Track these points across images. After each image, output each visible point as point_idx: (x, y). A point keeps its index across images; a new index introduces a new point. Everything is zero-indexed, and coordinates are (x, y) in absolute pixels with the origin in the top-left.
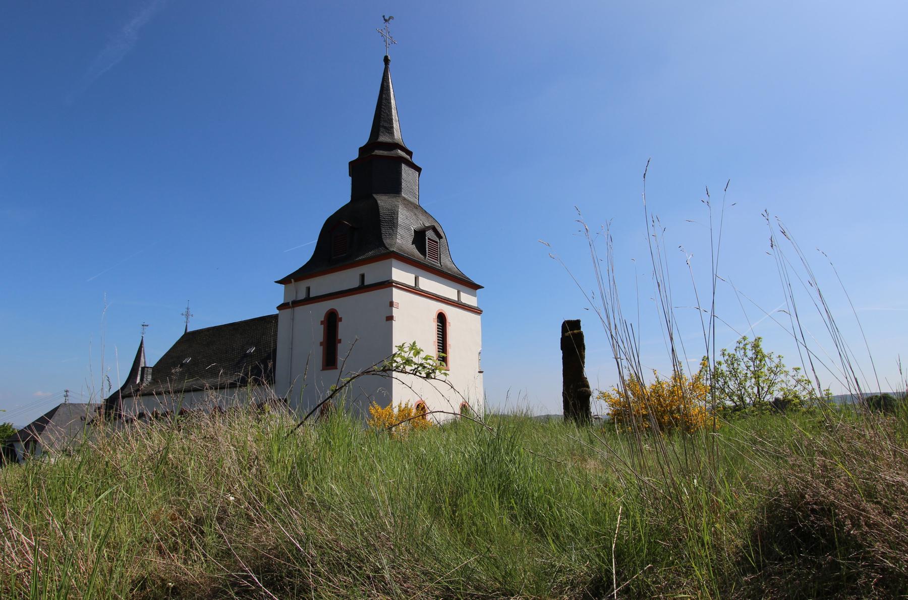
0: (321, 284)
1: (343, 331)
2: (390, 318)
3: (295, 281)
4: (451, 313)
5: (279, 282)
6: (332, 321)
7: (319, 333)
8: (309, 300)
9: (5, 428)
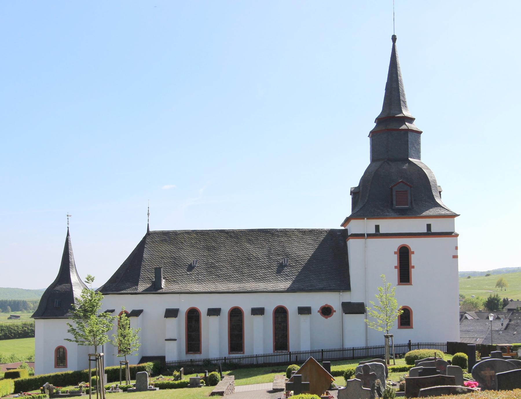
1: (414, 260)
2: (456, 257)
6: (404, 254)
7: (395, 260)
8: (377, 234)
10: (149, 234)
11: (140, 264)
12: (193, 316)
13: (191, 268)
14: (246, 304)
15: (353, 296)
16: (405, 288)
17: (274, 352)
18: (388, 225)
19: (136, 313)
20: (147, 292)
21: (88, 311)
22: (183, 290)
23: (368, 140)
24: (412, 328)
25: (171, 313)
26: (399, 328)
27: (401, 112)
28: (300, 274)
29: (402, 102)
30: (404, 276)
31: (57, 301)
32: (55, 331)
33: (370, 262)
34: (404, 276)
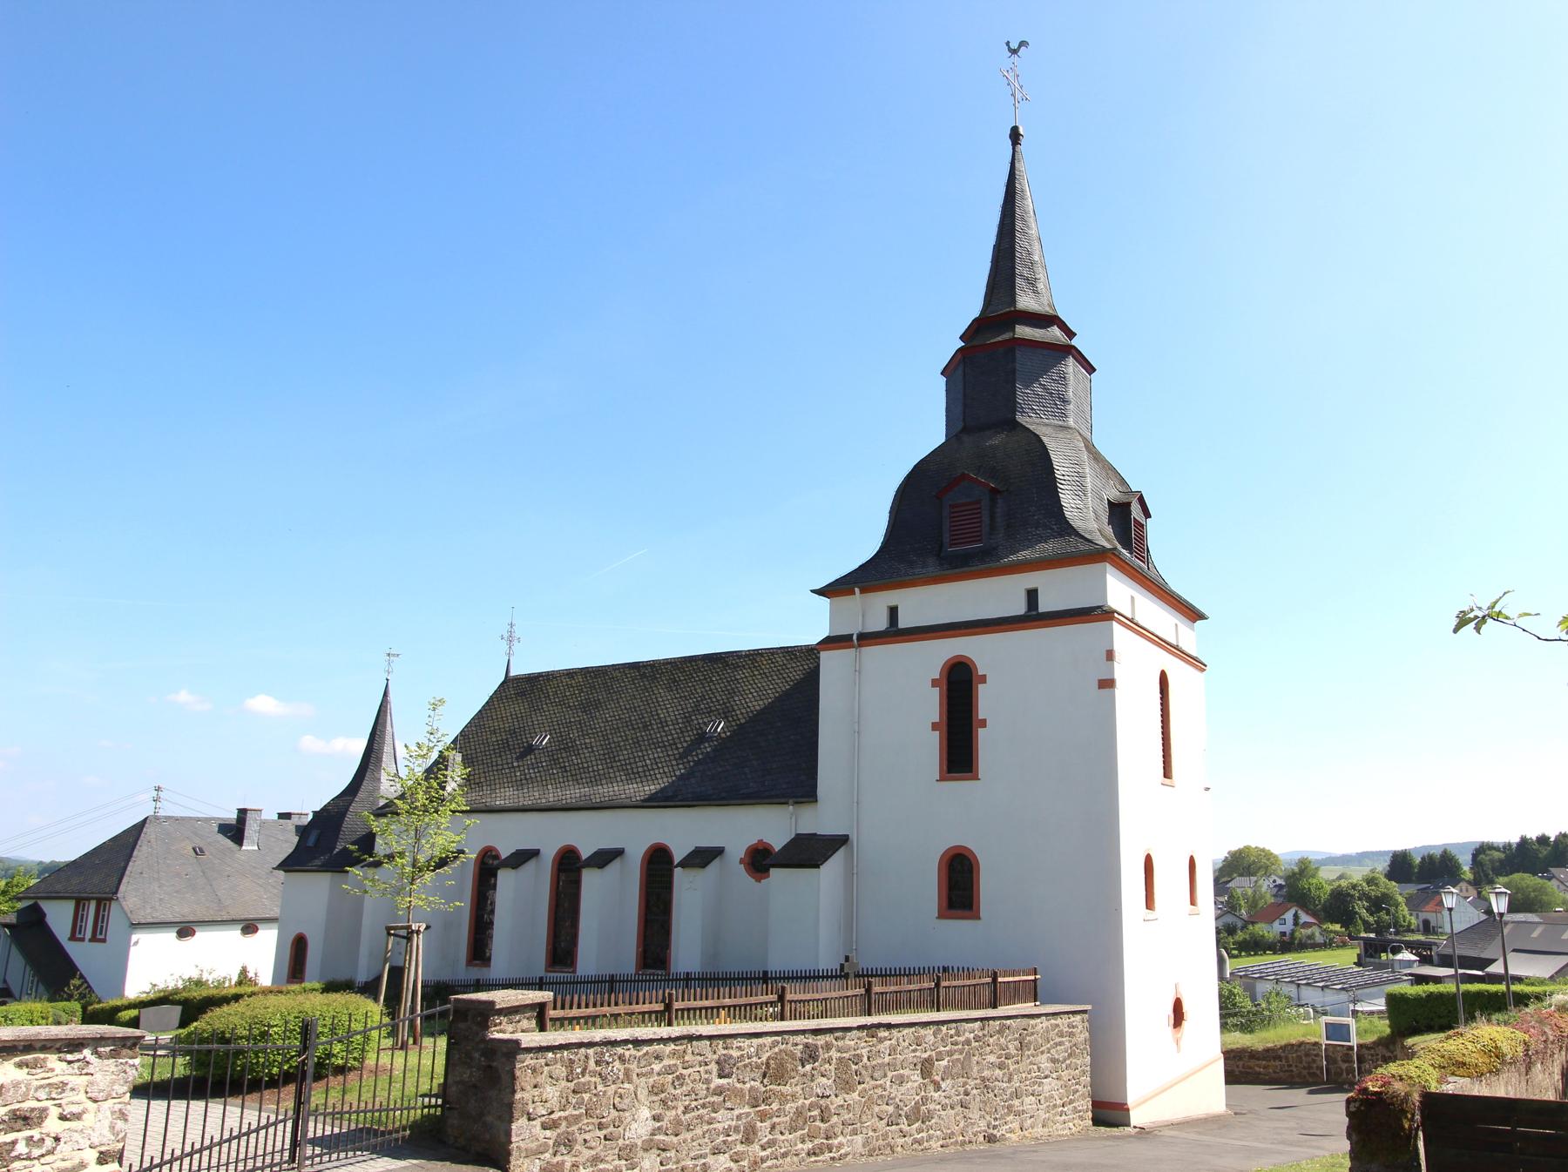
0: (922, 603)
1: (987, 701)
2: (1108, 684)
3: (862, 591)
4: (1179, 674)
5: (821, 592)
6: (959, 685)
7: (931, 705)
8: (895, 633)
9: (7, 869)
15: (818, 820)
16: (959, 788)
17: (637, 969)
23: (938, 388)
26: (941, 916)
27: (1014, 301)
29: (1018, 281)
30: (959, 756)
34: (959, 756)
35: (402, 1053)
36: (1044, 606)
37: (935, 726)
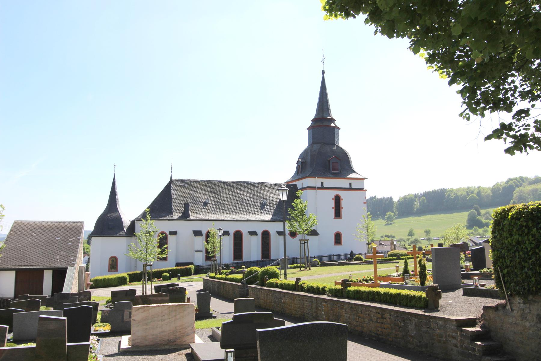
1: (343, 204)
6: (337, 200)
7: (332, 204)
8: (322, 188)
10: (171, 181)
11: (171, 201)
12: (238, 236)
13: (205, 204)
14: (245, 229)
16: (338, 220)
18: (329, 182)
19: (174, 233)
20: (179, 219)
21: (132, 230)
22: (204, 218)
24: (342, 245)
25: (197, 233)
28: (275, 210)
30: (338, 214)
31: (109, 224)
32: (115, 245)
33: (316, 203)
34: (338, 214)
35: (149, 282)
36: (325, 186)
37: (342, 208)
